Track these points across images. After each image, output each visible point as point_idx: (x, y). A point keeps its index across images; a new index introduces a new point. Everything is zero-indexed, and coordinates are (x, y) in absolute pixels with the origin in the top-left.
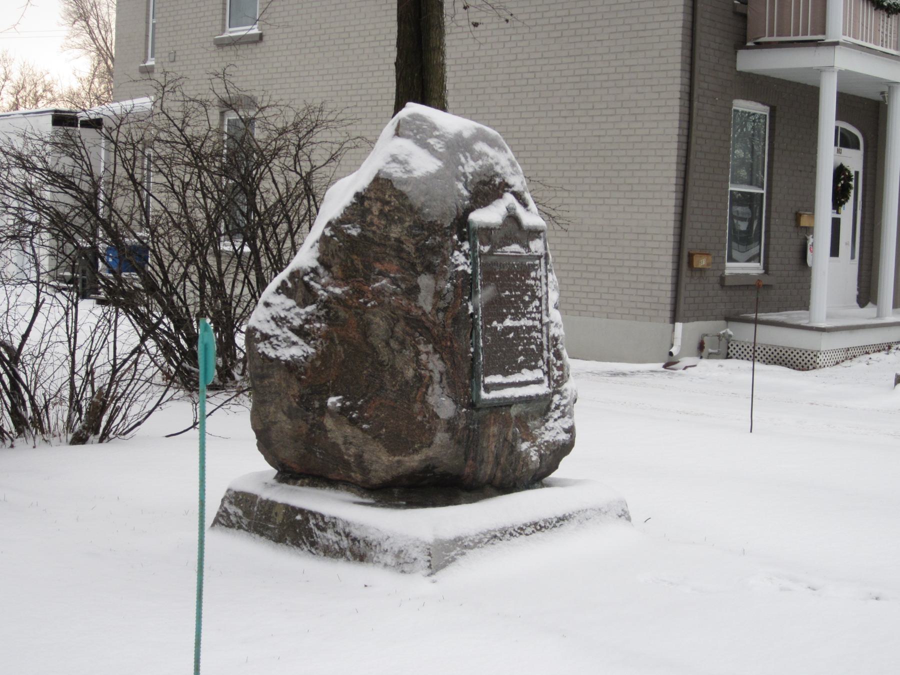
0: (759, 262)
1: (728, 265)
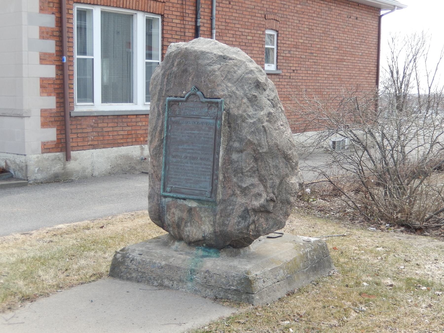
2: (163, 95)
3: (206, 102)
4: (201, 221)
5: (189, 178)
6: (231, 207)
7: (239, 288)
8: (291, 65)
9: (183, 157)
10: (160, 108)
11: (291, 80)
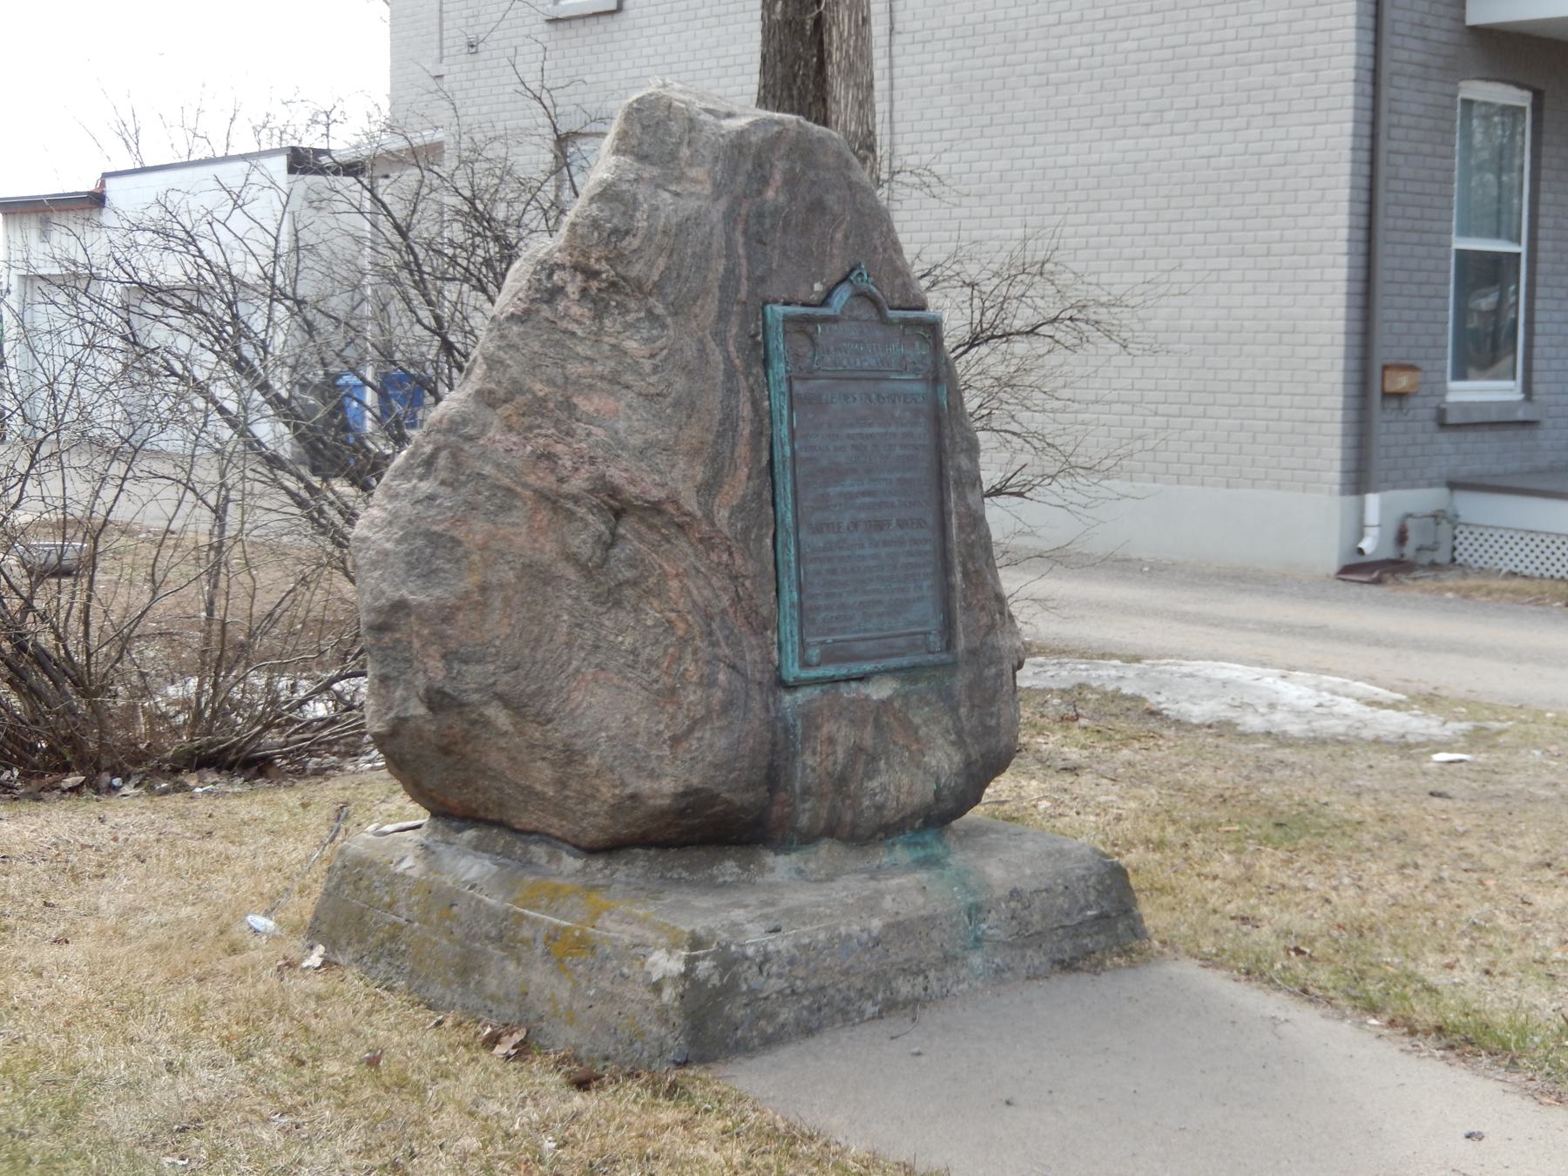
0: (1514, 378)
1: (1453, 385)
2: (743, 295)
4: (918, 740)
6: (993, 670)
7: (1106, 905)
9: (845, 525)
10: (732, 349)
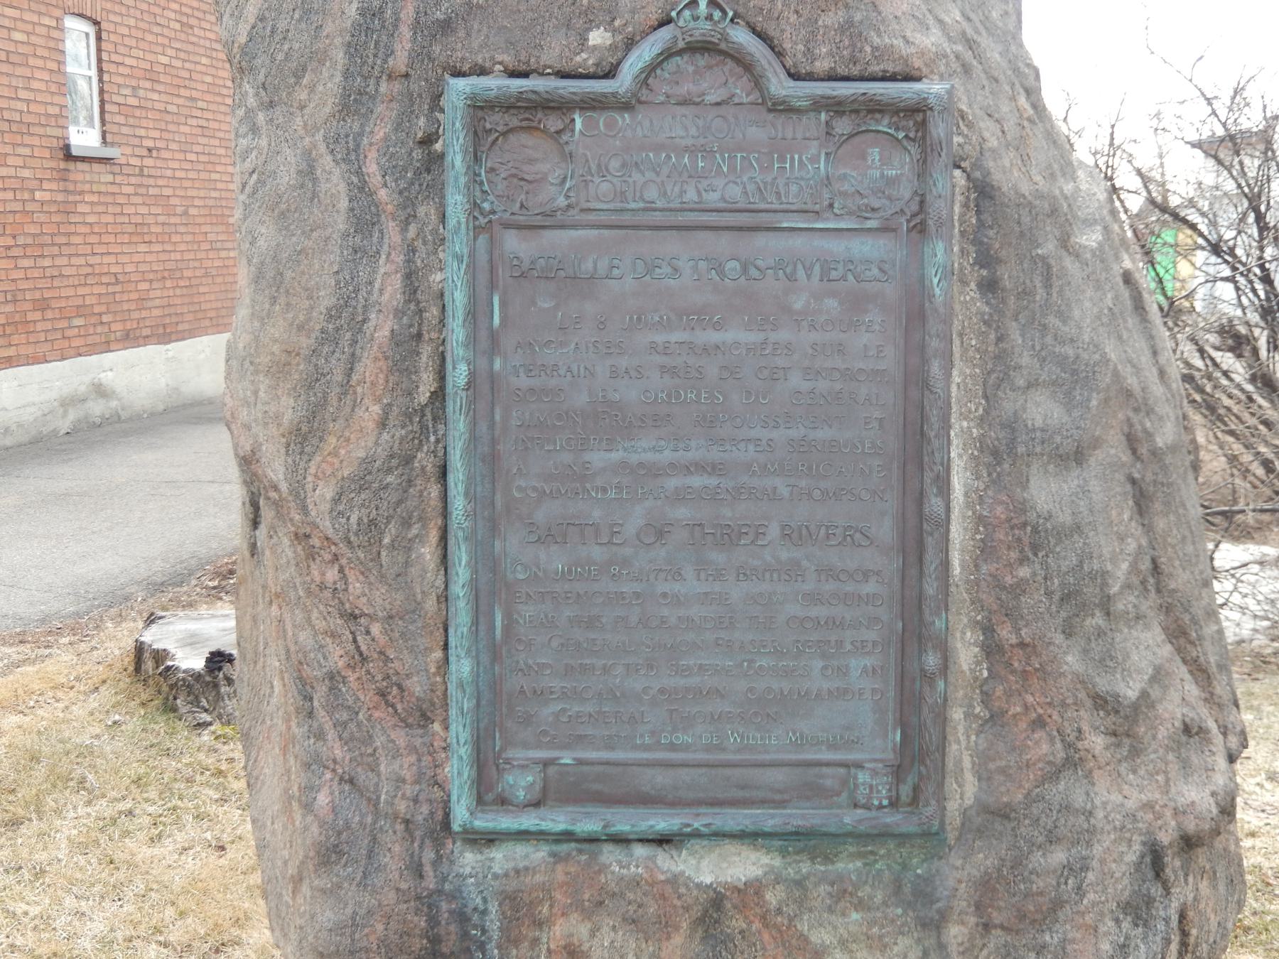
2: (400, 61)
3: (820, 104)
5: (694, 681)
6: (1059, 856)
8: (142, 132)
9: (631, 529)
10: (372, 168)
11: (146, 181)
